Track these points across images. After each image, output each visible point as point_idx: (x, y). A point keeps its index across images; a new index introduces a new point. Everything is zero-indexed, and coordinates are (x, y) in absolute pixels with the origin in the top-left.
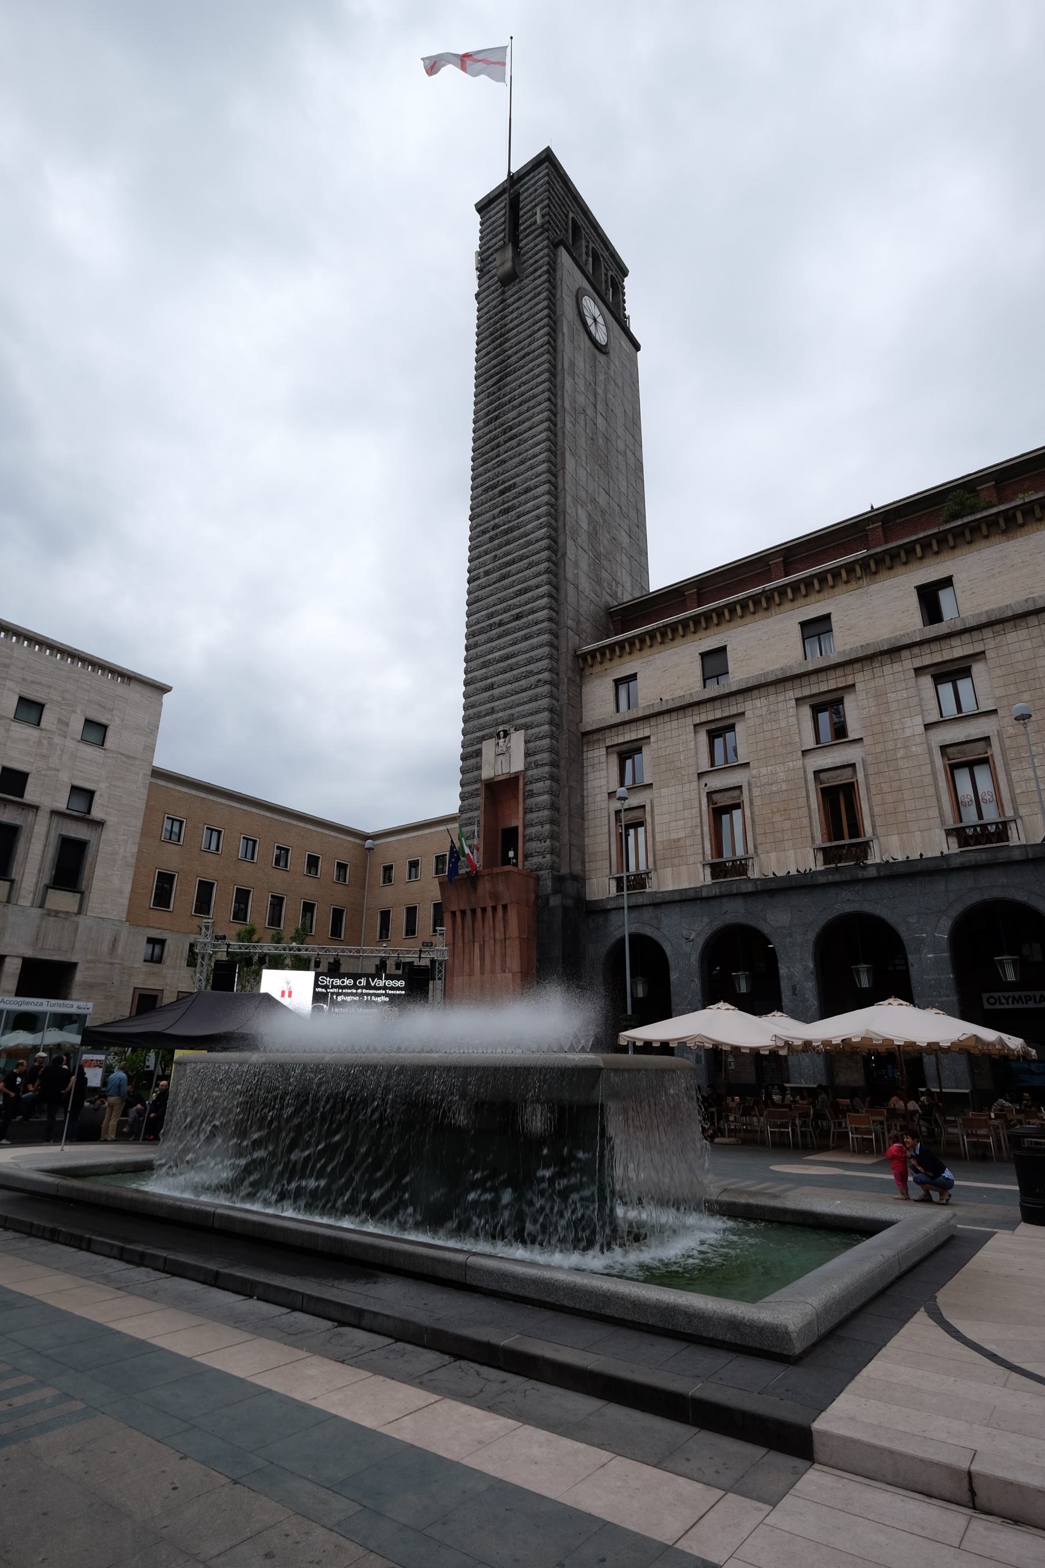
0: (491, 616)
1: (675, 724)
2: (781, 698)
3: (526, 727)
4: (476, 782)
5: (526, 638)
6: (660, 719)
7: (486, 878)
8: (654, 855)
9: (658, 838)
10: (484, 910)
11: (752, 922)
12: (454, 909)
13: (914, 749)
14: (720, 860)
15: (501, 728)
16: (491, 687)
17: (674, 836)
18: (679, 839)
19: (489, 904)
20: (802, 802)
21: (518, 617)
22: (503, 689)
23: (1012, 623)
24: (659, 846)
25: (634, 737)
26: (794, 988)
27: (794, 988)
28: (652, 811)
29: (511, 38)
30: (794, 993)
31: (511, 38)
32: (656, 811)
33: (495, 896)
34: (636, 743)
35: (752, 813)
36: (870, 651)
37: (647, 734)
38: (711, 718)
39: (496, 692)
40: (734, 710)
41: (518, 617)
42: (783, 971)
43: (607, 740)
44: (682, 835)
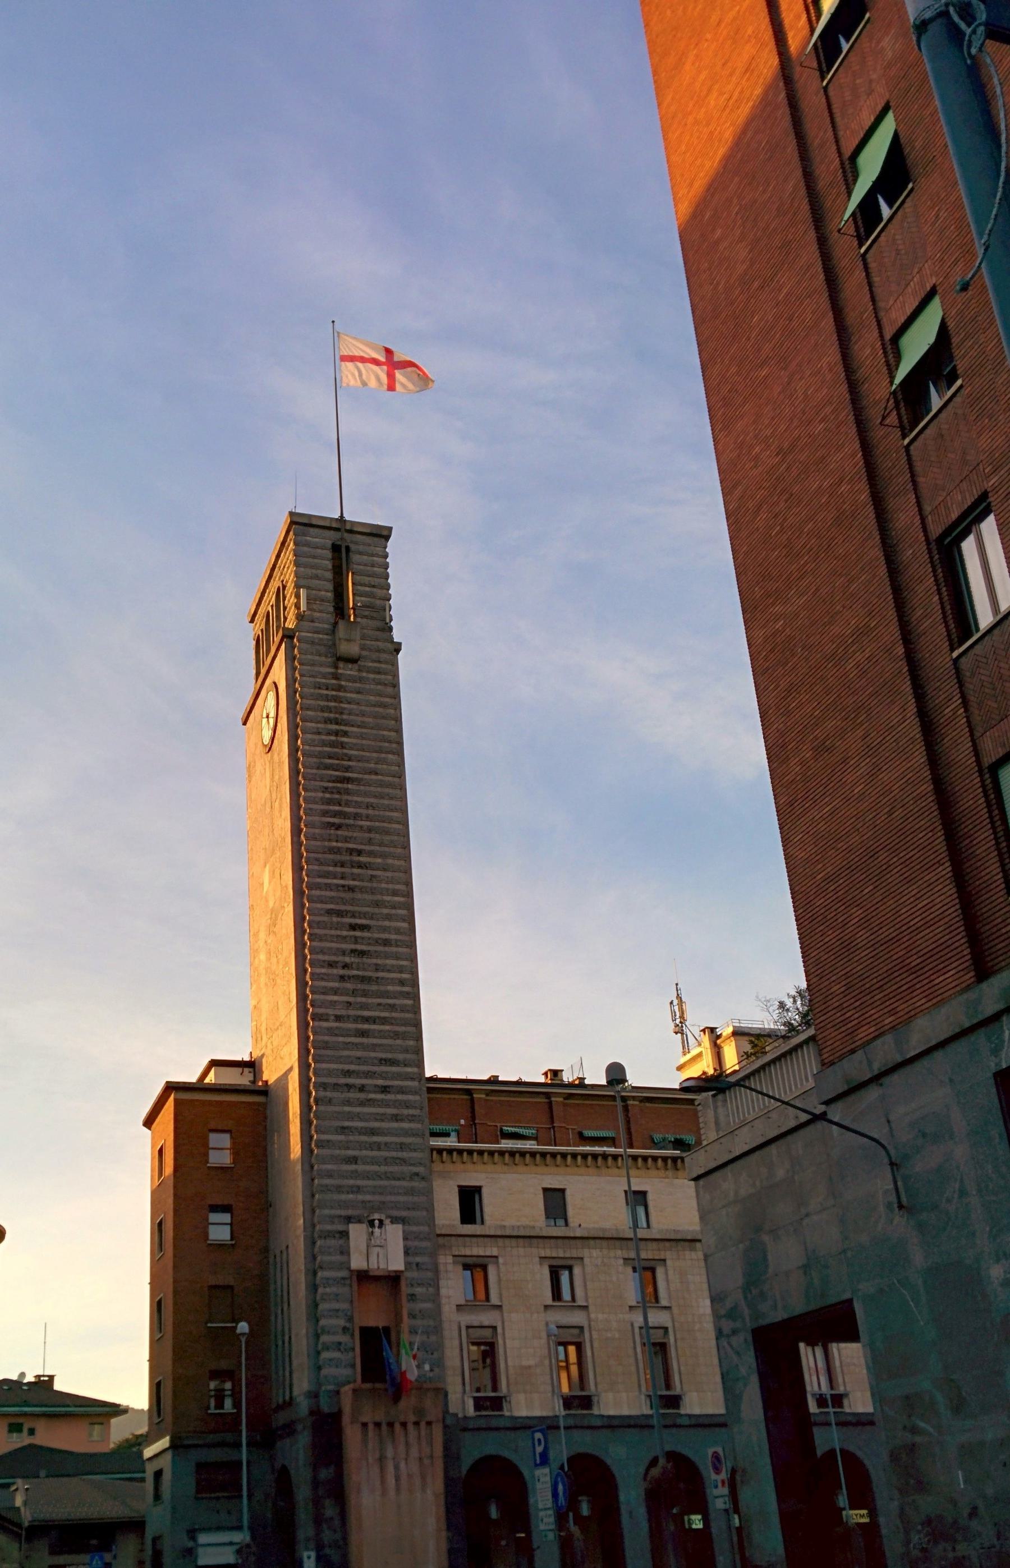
0: (348, 1073)
1: (521, 1251)
2: (612, 1254)
3: (403, 1221)
4: (340, 1269)
5: (396, 1118)
6: (507, 1241)
7: (414, 1392)
8: (507, 1378)
9: (510, 1363)
10: (404, 1425)
11: (596, 1452)
12: (365, 1420)
13: (705, 1325)
14: (584, 1393)
15: (376, 1216)
16: (354, 1160)
17: (525, 1363)
18: (530, 1367)
19: (412, 1418)
20: (631, 1352)
21: (385, 1089)
22: (368, 1168)
23: (240, 1070)
24: (511, 1371)
25: (482, 1253)
26: (631, 1513)
27: (631, 1513)
28: (504, 1334)
29: (333, 322)
30: (631, 1517)
31: (333, 322)
32: (507, 1335)
33: (420, 1412)
34: (481, 1259)
35: (593, 1353)
36: (679, 1237)
37: (495, 1253)
38: (554, 1255)
39: (360, 1168)
40: (574, 1253)
41: (385, 1089)
42: (622, 1498)
43: (454, 1248)
44: (532, 1362)
